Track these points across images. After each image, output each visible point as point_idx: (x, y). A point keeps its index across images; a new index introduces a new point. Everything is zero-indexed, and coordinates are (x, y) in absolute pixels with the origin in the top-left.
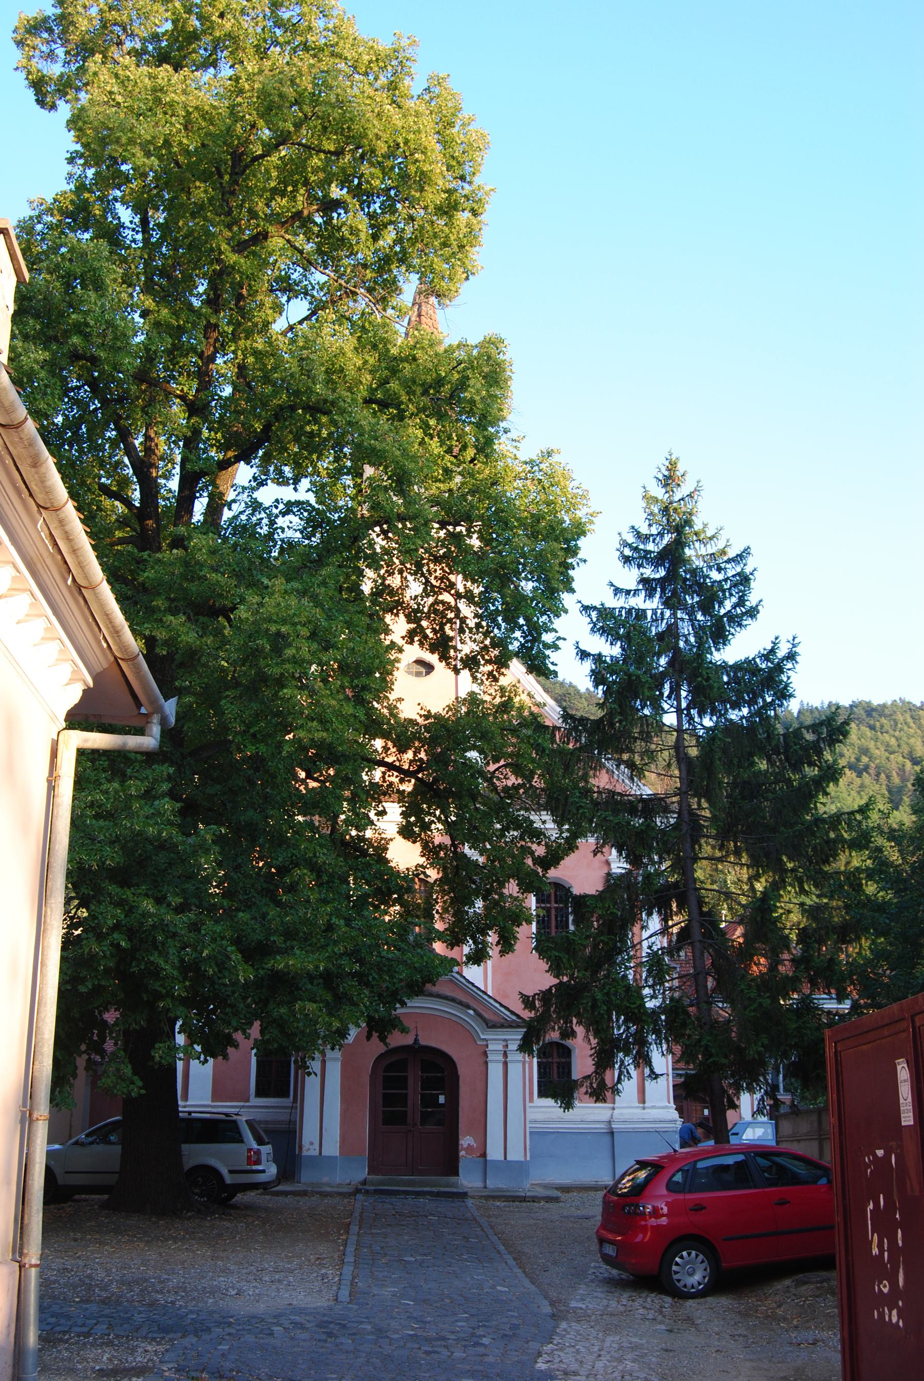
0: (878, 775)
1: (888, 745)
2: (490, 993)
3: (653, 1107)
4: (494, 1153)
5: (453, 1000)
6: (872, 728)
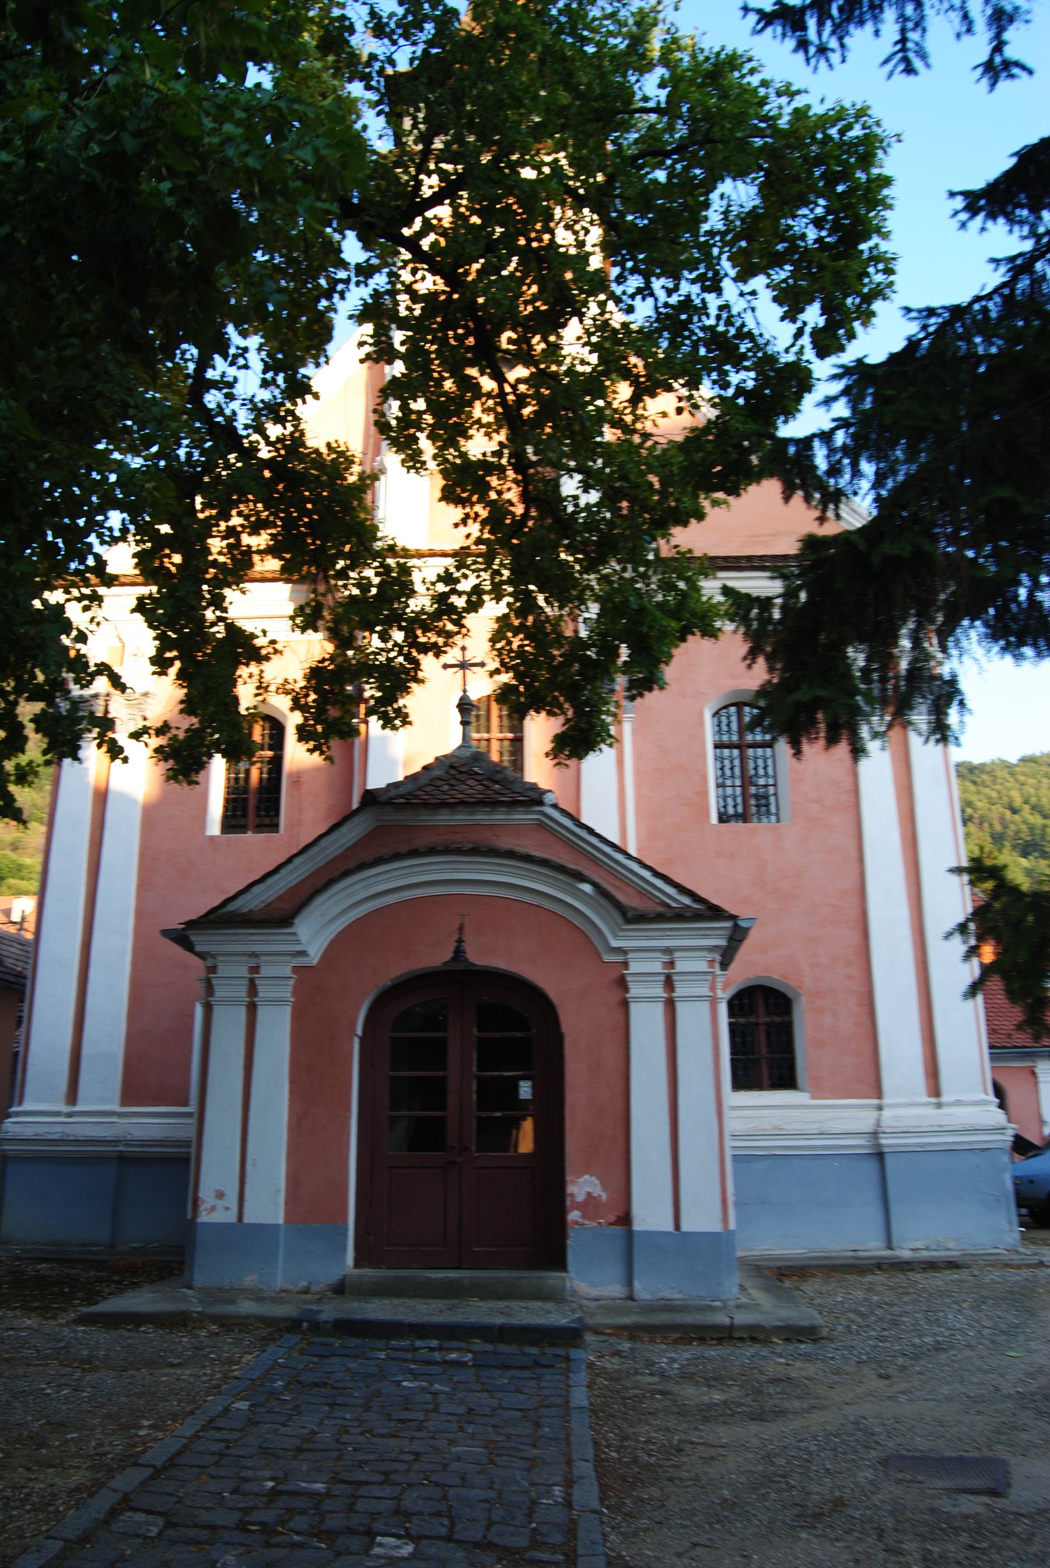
0: (981, 823)
1: (990, 798)
2: (632, 851)
3: (958, 1103)
4: (650, 1214)
5: (544, 863)
6: (974, 783)
